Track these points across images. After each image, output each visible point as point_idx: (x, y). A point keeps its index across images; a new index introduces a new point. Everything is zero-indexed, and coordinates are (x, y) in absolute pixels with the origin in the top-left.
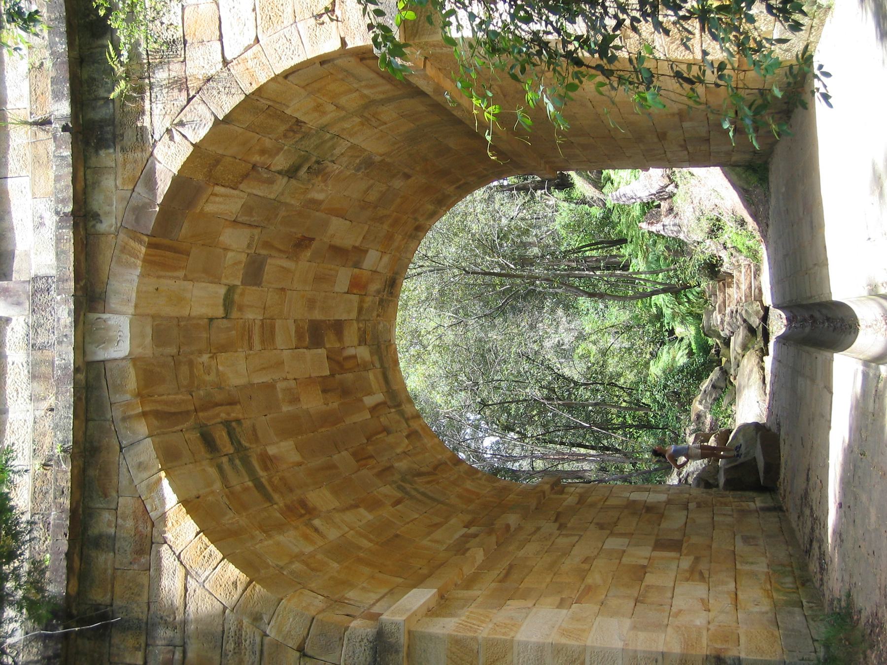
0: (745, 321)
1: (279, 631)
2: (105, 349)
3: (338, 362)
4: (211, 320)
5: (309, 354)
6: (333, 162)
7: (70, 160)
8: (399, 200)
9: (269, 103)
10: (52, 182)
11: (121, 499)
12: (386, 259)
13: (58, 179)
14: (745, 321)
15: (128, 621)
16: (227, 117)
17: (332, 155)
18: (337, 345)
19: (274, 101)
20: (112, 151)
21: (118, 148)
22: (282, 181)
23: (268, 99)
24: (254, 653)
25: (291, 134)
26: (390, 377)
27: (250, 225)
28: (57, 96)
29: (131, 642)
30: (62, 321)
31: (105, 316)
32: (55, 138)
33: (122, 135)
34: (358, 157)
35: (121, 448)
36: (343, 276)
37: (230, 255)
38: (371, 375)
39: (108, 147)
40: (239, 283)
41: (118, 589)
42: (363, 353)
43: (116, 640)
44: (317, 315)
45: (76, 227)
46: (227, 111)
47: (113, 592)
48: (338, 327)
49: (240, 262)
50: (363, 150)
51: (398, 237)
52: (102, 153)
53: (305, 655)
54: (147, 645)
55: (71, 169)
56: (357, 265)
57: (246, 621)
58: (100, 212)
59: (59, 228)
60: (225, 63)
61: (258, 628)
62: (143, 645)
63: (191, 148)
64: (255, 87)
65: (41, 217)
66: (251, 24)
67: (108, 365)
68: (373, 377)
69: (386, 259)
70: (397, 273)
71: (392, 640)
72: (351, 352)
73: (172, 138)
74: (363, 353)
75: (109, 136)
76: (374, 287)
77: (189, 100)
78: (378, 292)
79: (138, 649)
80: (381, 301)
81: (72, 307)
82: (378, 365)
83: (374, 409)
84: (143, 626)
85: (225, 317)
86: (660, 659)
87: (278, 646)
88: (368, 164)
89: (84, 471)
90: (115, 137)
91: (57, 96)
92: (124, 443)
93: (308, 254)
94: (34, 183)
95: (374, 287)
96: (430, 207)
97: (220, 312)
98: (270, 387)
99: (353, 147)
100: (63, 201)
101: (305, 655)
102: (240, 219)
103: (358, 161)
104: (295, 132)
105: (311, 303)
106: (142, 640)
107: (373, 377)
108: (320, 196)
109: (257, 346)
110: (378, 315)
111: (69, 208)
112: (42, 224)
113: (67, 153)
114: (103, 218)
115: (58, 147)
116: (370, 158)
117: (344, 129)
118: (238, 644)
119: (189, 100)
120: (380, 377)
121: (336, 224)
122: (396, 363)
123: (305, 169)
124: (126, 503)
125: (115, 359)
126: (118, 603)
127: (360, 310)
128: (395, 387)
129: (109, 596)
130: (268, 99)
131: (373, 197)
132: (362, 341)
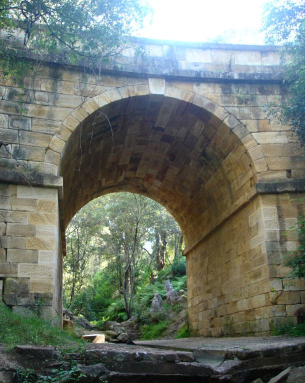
0: (120, 334)
1: (55, 141)
2: (153, 85)
3: (124, 167)
4: (154, 122)
5: (129, 158)
6: (205, 169)
7: (218, 78)
8: (181, 194)
9: (235, 147)
10: (211, 70)
11: (100, 86)
12: (156, 189)
13: (212, 73)
14: (120, 334)
15: (57, 86)
16: (233, 133)
17: (208, 169)
18: (128, 168)
19: (235, 150)
20: (221, 92)
21: (222, 94)
22: (200, 150)
23: (237, 147)
24: (47, 131)
25: (220, 154)
26: (110, 189)
27: (185, 138)
28: (240, 75)
29: (49, 86)
30: (163, 70)
31: (164, 85)
32: (226, 73)
33: (226, 96)
34: (205, 178)
35: (117, 88)
36: (154, 172)
37: (176, 131)
38: (112, 181)
39: (222, 91)
40: (164, 133)
41: (68, 83)
42: (121, 179)
43: (49, 81)
44: (142, 161)
45: (196, 78)
46: (235, 133)
47: (67, 81)
48: (134, 170)
49: (172, 134)
50: (207, 180)
51: (164, 194)
52: (220, 89)
53: (46, 150)
54: (48, 92)
55: (215, 78)
56: (157, 177)
57: (58, 129)
58: (200, 87)
59: (196, 72)
60: (251, 133)
61: (55, 133)
62: (48, 91)
63: (222, 120)
64: (243, 142)
65: (198, 66)
66: (264, 142)
67: (147, 85)
68: (111, 182)
69: (156, 189)
70: (148, 193)
71: (55, 181)
72: (123, 174)
73: (225, 113)
74: (121, 179)
75: (226, 91)
76: (146, 184)
77: (238, 120)
78: (143, 186)
79: (46, 89)
80: (139, 187)
81: (168, 75)
82: (115, 184)
83: (100, 182)
84: (55, 91)
85: (153, 127)
86: (51, 277)
87: (50, 140)
88: (201, 182)
89: (107, 73)
90: (226, 93)
91: (240, 75)
92: (120, 89)
93: (168, 159)
94: (210, 64)
95: (146, 184)
96: (174, 207)
97: (156, 125)
98: (123, 143)
99: (210, 176)
100: (205, 74)
101: (46, 150)
102: (189, 135)
103: (203, 178)
104: (221, 156)
105: (147, 159)
106: (49, 90)
107: (111, 182)
108: (191, 164)
109: (138, 138)
110: (133, 185)
111: (202, 76)
112: (196, 66)
113: (221, 76)
114: (197, 87)
115: (223, 74)
116: (203, 183)
117: (218, 173)
118: (50, 126)
119: (238, 120)
120: (110, 185)
121: (177, 170)
122: (113, 192)
123: (204, 159)
124: (99, 88)
125: (149, 88)
126: (63, 83)
127: (138, 178)
128: (104, 191)
129: (65, 80)
130: (237, 147)
131: (185, 184)
132: (126, 179)
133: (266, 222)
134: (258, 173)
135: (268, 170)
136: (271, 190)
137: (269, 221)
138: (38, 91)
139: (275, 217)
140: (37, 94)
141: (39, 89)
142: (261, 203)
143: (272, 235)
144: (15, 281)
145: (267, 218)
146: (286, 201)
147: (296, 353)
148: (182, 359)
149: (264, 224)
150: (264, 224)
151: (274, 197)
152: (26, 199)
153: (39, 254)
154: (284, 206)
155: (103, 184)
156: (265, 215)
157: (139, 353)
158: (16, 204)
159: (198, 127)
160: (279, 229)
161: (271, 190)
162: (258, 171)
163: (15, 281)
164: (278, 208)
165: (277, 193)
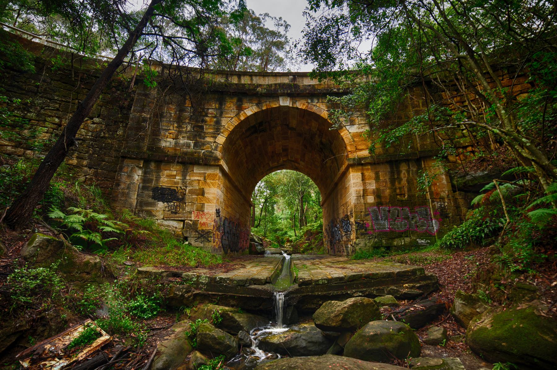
56: (301, 160)
68: (276, 164)
107: (276, 164)
133: (354, 184)
134: (349, 152)
135: (357, 149)
136: (359, 164)
137: (356, 183)
138: (211, 109)
139: (360, 180)
140: (210, 111)
141: (211, 107)
142: (351, 171)
143: (358, 192)
144: (190, 222)
145: (355, 181)
146: (368, 169)
147: (342, 283)
148: (255, 282)
149: (352, 185)
150: (352, 185)
151: (360, 167)
152: (199, 173)
153: (206, 206)
154: (367, 174)
155: (271, 165)
156: (354, 179)
157: (219, 278)
158: (193, 176)
159: (314, 125)
160: (362, 188)
161: (359, 164)
162: (350, 150)
163: (190, 222)
164: (363, 174)
165: (362, 165)
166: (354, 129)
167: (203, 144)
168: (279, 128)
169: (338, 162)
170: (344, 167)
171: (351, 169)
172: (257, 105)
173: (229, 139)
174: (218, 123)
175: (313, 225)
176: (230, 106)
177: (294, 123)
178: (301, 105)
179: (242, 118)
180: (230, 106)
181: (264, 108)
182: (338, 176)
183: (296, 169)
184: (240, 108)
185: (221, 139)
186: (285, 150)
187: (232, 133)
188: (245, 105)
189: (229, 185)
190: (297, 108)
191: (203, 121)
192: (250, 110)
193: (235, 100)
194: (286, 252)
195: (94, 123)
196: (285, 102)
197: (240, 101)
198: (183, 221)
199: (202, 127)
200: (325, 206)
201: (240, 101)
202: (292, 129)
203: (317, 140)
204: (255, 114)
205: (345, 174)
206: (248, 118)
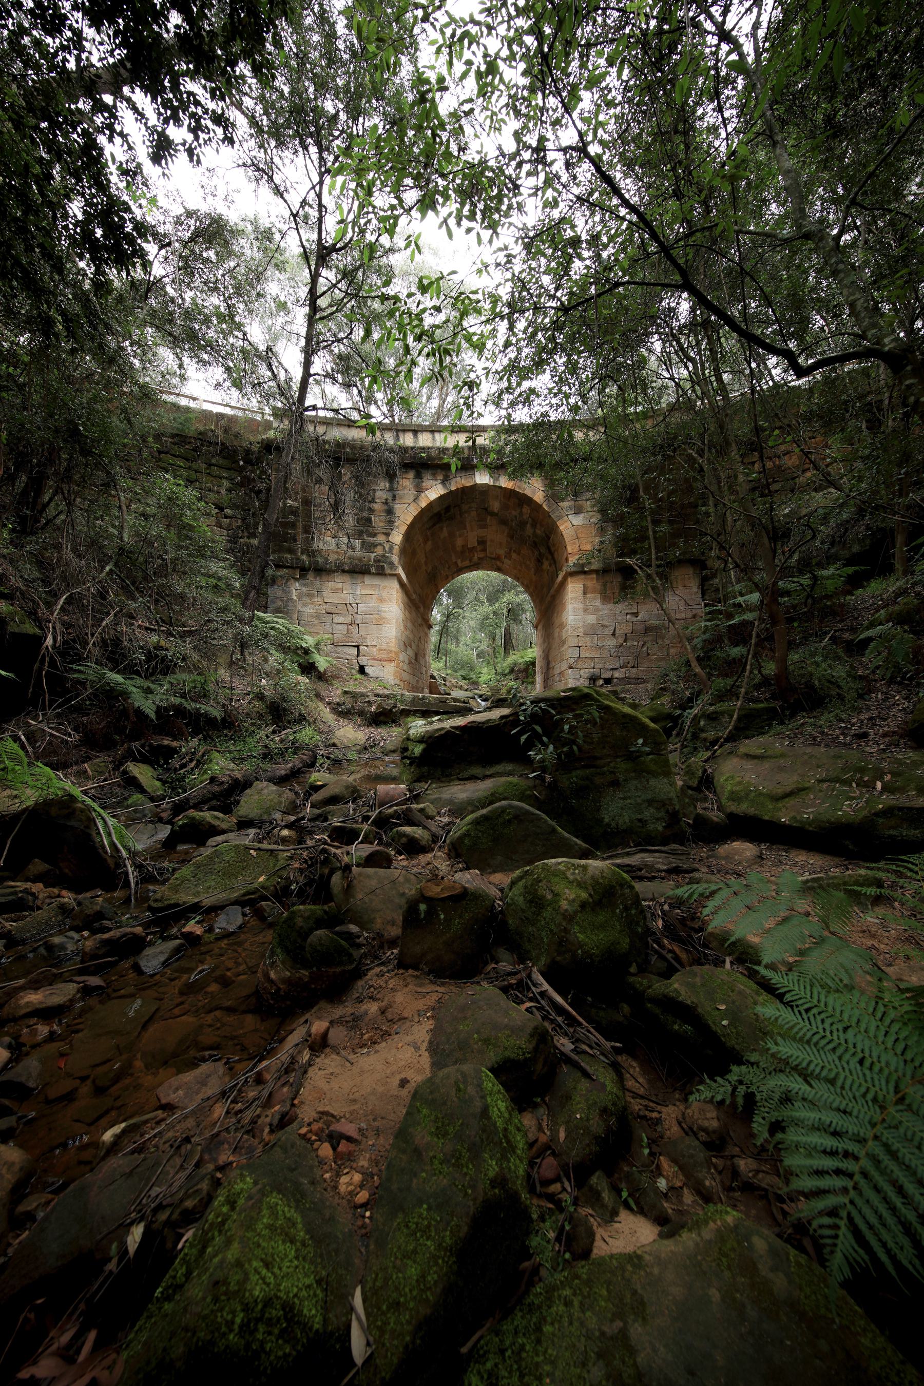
3: (472, 550)
107: (467, 563)
151: (583, 576)
161: (580, 571)
165: (585, 573)
166: (578, 520)
167: (375, 545)
168: (474, 514)
169: (556, 565)
170: (560, 578)
171: (569, 579)
172: (444, 482)
173: (408, 536)
174: (390, 512)
175: (518, 657)
176: (406, 482)
177: (495, 506)
178: (504, 482)
179: (423, 504)
180: (406, 482)
181: (453, 488)
182: (556, 586)
183: (499, 570)
184: (420, 490)
185: (397, 538)
186: (482, 542)
187: (411, 527)
188: (427, 483)
189: (406, 599)
190: (501, 487)
191: (371, 510)
192: (434, 491)
193: (411, 475)
194: (480, 696)
195: (226, 517)
196: (482, 478)
197: (419, 476)
198: (358, 647)
199: (369, 520)
200: (540, 627)
201: (419, 476)
202: (493, 514)
203: (529, 530)
204: (441, 497)
205: (563, 584)
206: (431, 505)
